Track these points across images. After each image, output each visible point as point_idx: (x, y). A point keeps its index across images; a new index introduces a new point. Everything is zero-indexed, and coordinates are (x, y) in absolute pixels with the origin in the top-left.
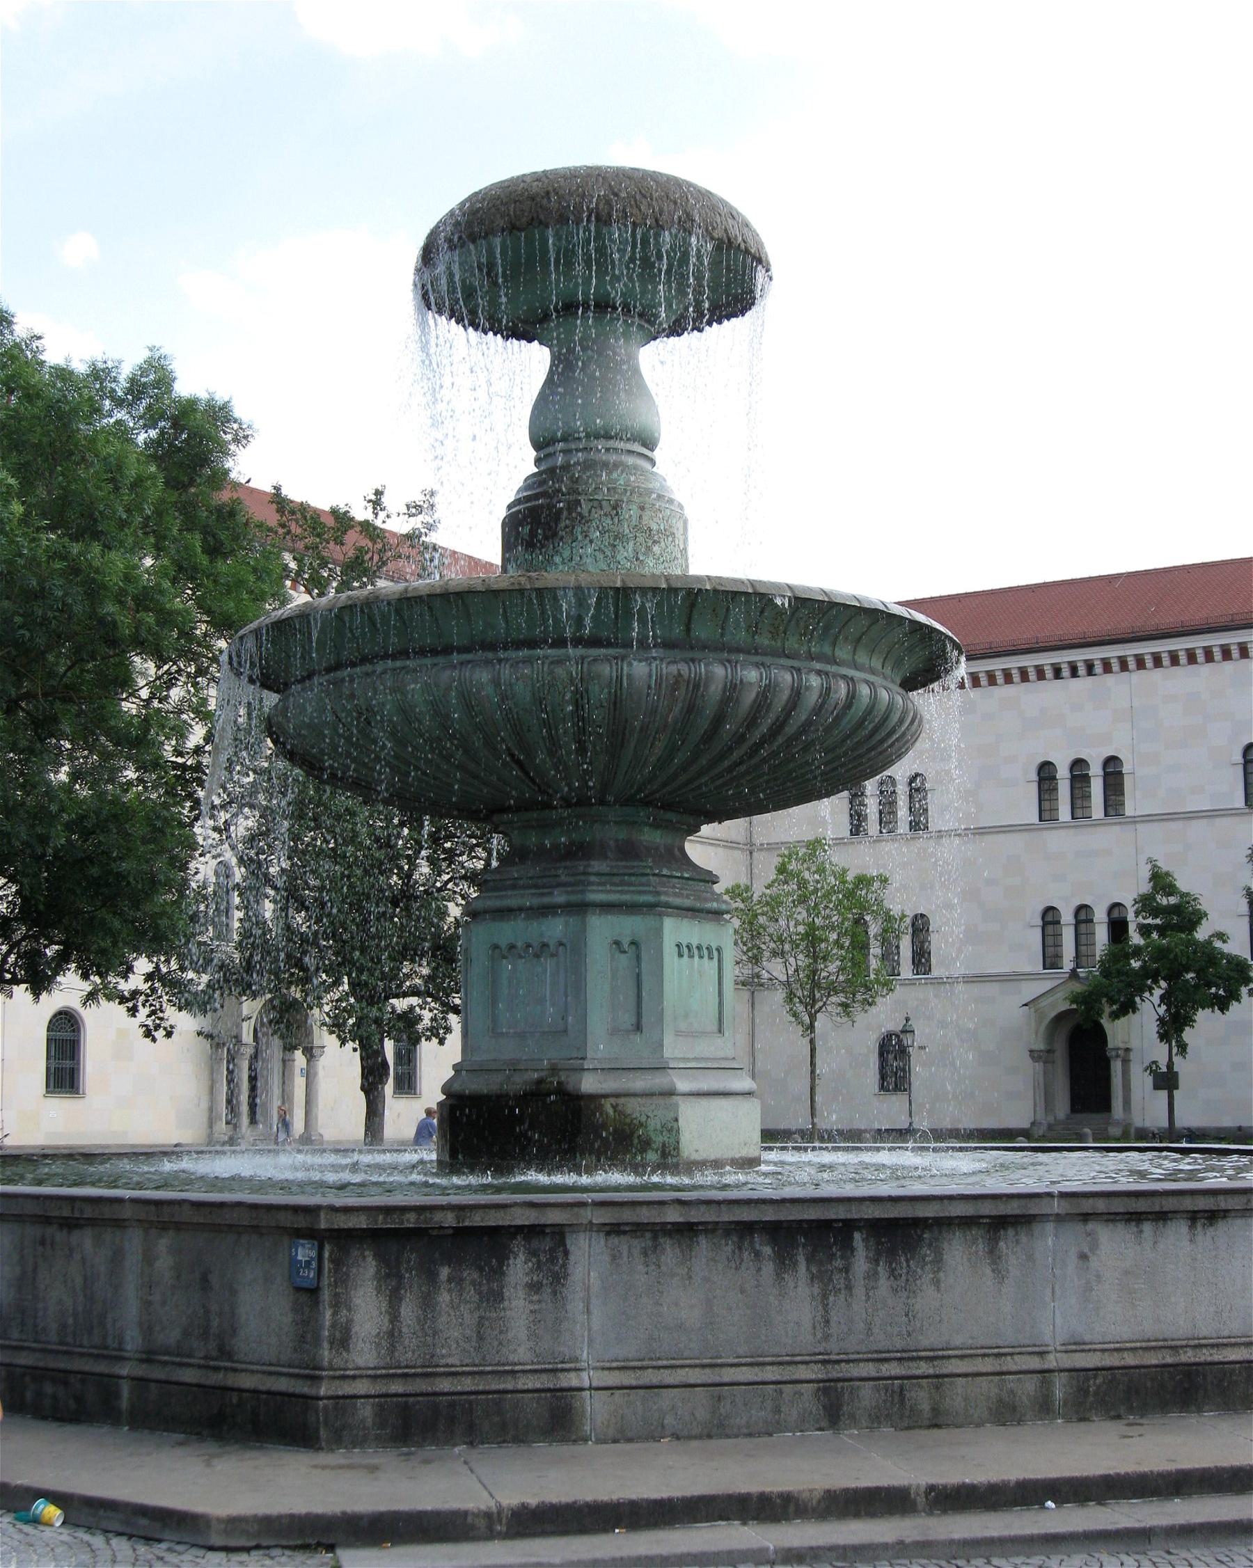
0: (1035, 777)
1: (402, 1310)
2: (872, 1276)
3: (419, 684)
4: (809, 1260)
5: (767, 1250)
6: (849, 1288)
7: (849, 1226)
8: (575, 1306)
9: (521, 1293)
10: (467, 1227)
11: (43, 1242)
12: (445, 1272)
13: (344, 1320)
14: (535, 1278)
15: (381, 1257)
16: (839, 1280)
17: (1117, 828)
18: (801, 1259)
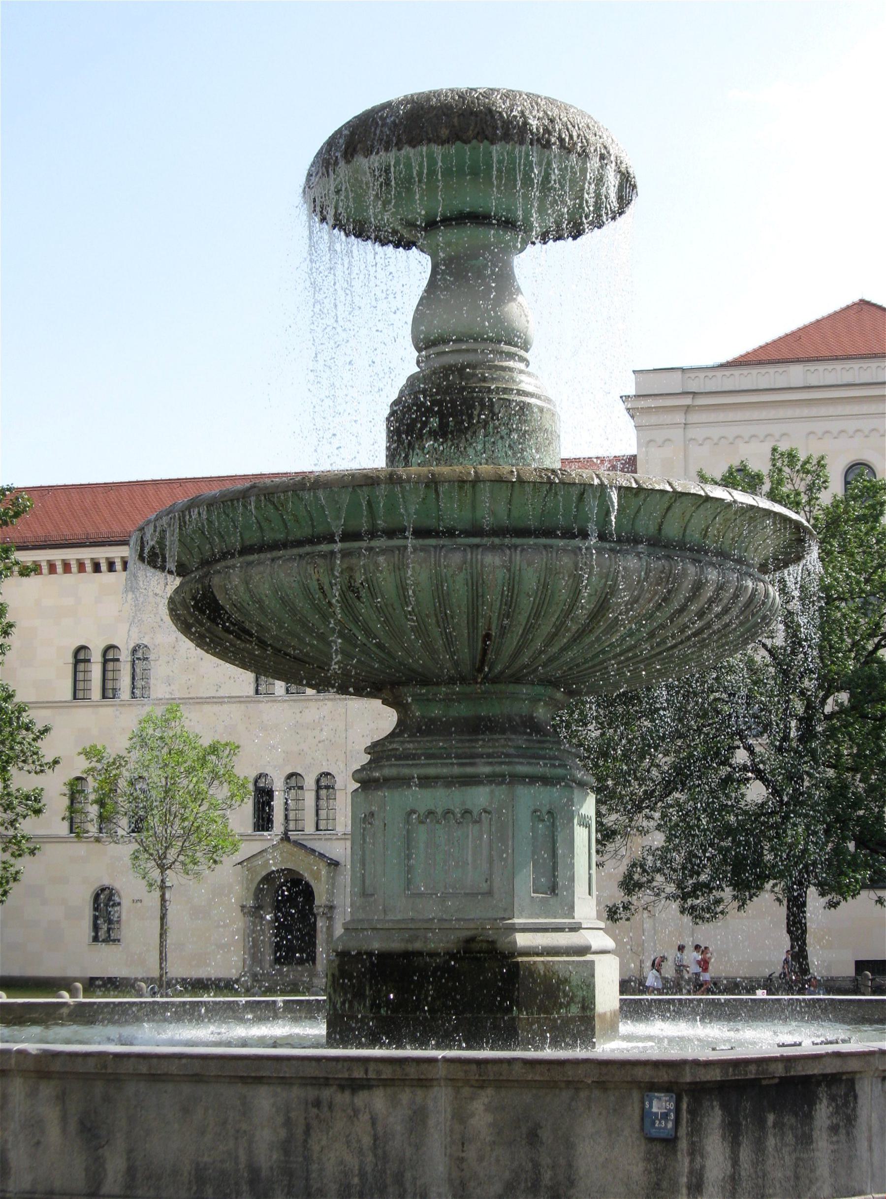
1: (741, 1154)
8: (862, 1145)
9: (825, 1136)
10: (793, 1077)
11: (317, 1104)
12: (771, 1118)
13: (698, 1167)
14: (835, 1121)
15: (723, 1107)
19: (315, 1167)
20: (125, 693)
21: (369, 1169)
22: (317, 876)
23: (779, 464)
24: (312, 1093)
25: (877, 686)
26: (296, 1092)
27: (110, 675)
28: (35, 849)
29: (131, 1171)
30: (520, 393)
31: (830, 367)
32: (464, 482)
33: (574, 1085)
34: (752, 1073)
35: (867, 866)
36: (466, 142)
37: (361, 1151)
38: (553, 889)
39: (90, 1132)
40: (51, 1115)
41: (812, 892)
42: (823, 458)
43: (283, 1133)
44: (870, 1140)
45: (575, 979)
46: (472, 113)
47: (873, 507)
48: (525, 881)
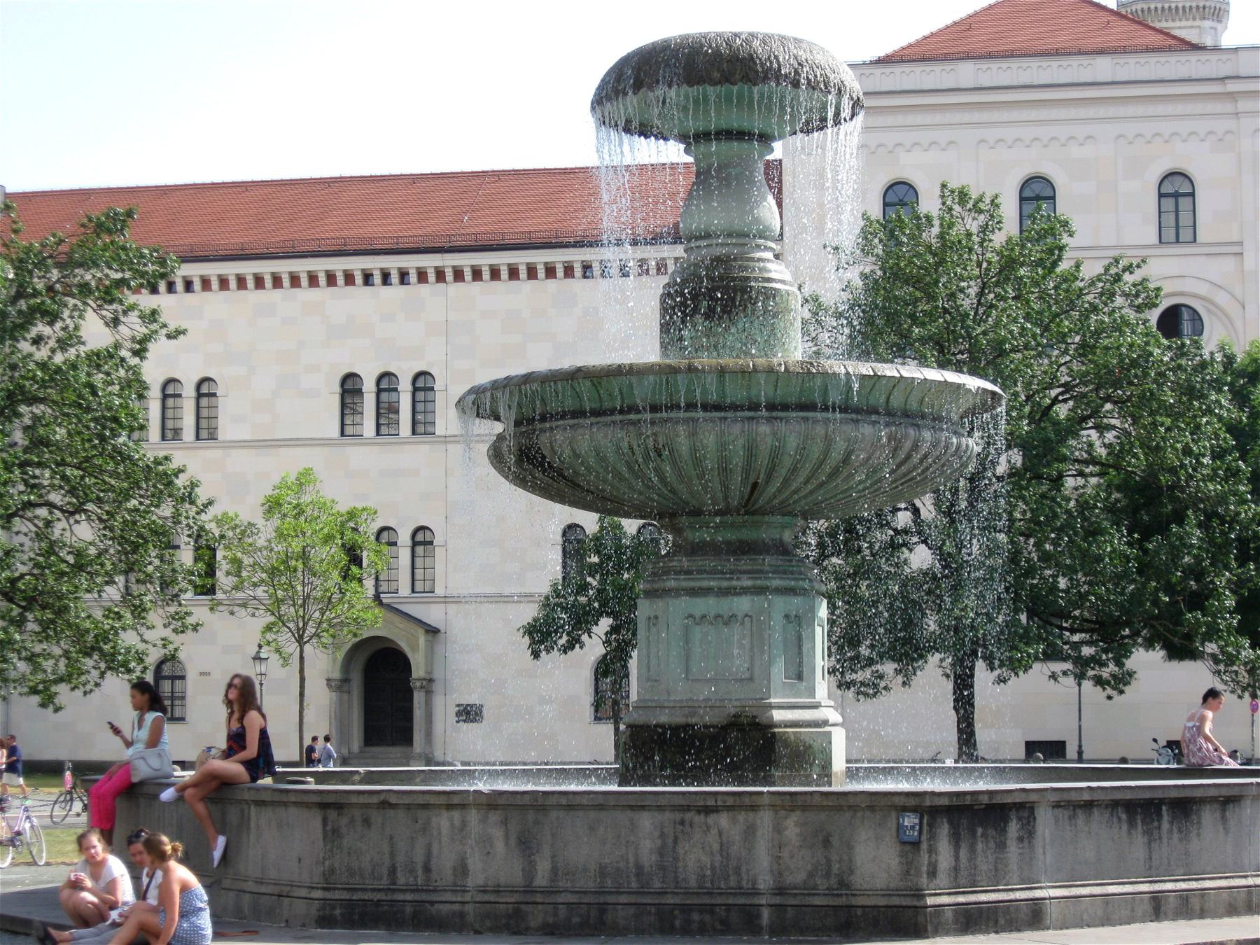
0: (338, 389)
2: (1170, 831)
3: (712, 437)
4: (1143, 823)
5: (1124, 816)
6: (1160, 838)
7: (1162, 801)
12: (980, 831)
15: (950, 823)
16: (1155, 832)
17: (425, 449)
18: (1139, 822)
19: (680, 864)
20: (188, 433)
21: (717, 865)
22: (415, 648)
23: (949, 203)
24: (678, 816)
25: (1052, 449)
26: (668, 815)
27: (170, 413)
28: (198, 625)
29: (554, 871)
30: (769, 280)
31: (1004, 66)
32: (744, 372)
33: (853, 808)
34: (968, 800)
35: (1040, 639)
36: (734, 84)
37: (712, 854)
38: (800, 677)
39: (526, 845)
40: (498, 834)
41: (980, 665)
42: (996, 196)
43: (659, 842)
44: (1044, 848)
45: (816, 745)
46: (738, 59)
47: (1050, 252)
48: (779, 669)
